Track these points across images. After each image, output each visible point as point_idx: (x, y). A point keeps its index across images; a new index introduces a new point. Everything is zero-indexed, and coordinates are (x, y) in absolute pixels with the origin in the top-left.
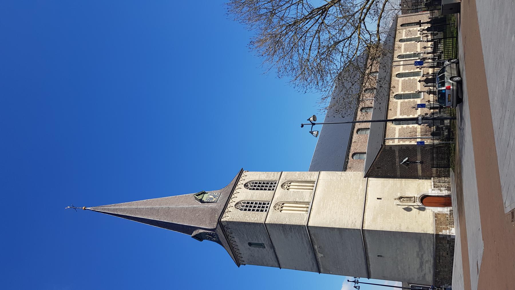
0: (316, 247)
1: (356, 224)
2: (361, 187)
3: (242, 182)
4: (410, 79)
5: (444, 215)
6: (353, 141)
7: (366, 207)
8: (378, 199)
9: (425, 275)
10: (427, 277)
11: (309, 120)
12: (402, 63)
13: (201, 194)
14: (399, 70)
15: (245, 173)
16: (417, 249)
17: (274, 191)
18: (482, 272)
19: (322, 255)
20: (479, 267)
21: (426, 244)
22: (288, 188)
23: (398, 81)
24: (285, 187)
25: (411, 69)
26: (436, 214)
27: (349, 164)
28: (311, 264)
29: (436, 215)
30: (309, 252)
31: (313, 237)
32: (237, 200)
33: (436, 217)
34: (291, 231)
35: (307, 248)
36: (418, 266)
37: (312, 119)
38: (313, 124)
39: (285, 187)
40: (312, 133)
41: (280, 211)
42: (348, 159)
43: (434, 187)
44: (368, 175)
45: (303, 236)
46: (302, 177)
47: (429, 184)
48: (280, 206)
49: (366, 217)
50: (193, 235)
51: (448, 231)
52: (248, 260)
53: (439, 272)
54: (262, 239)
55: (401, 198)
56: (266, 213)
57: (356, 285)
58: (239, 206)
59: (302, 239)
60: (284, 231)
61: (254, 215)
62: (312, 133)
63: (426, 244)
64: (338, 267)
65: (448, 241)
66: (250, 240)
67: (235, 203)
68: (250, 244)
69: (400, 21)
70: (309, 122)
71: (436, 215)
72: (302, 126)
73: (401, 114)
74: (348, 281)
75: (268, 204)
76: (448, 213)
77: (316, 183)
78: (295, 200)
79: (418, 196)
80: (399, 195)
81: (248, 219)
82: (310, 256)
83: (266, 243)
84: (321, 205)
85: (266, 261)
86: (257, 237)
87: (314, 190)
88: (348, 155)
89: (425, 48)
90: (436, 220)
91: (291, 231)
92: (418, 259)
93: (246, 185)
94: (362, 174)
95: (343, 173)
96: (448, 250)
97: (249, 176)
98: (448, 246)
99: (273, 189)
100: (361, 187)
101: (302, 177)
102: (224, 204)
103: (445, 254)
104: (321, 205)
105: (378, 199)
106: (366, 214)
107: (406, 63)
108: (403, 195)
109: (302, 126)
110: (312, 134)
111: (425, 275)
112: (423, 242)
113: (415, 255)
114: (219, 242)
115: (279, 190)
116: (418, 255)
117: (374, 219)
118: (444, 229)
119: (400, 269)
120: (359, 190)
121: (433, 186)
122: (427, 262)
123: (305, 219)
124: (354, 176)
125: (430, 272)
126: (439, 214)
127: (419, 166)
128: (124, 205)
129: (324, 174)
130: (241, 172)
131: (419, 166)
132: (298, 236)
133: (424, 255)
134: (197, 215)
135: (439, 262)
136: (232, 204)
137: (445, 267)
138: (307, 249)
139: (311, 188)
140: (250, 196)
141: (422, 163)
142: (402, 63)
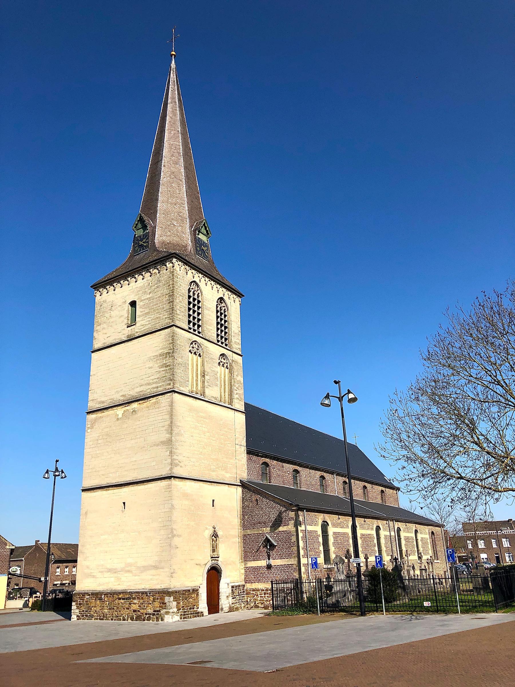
0: (135, 405)
1: (178, 467)
2: (228, 475)
3: (227, 295)
4: (375, 546)
5: (196, 604)
6: (284, 464)
7: (201, 484)
8: (213, 501)
9: (94, 577)
10: (91, 580)
11: (349, 392)
12: (393, 534)
13: (207, 231)
14: (385, 530)
15: (238, 300)
16: (141, 563)
17: (216, 342)
18: (197, 669)
19: (120, 416)
20: (208, 665)
21: (150, 577)
22: (221, 364)
23: (372, 529)
24: (223, 360)
25: (386, 547)
26: (198, 590)
27: (254, 458)
28: (103, 399)
29: (195, 591)
30: (123, 396)
31: (153, 400)
32: (202, 285)
33: (193, 590)
34: (162, 367)
35: (134, 393)
36: (109, 566)
37: (351, 396)
38: (341, 399)
39: (223, 360)
40: (327, 397)
41: (190, 351)
42: (262, 457)
43: (233, 587)
44: (243, 485)
45: (154, 386)
46: (237, 385)
47: (236, 579)
48: (196, 350)
49: (188, 482)
50: (143, 215)
51: (175, 610)
52: (105, 301)
53: (101, 599)
54: (143, 323)
55: (215, 535)
56: (187, 328)
57: (51, 474)
58: (193, 286)
59: (149, 384)
60: (160, 355)
61: (183, 310)
62: (327, 397)
63: (150, 577)
64: (99, 442)
65: (159, 611)
66: (142, 303)
67: (198, 281)
68: (133, 304)
69: (436, 530)
70: (344, 392)
71: (195, 591)
72: (336, 382)
73: (334, 533)
74: (57, 461)
75: (199, 333)
76: (200, 610)
77: (230, 406)
78: (206, 373)
79: (219, 563)
80: (220, 533)
81: (178, 301)
82: (118, 398)
83: (137, 329)
84: (201, 414)
85: (104, 328)
86: (148, 313)
87: (220, 404)
88: (266, 457)
89: (413, 568)
90: (189, 591)
91: (162, 367)
92: (122, 565)
93: (221, 299)
94: (244, 475)
95: (244, 449)
96: (142, 611)
97: (234, 305)
98: (150, 611)
99: (218, 341)
100: (228, 475)
101: (237, 385)
102: (196, 264)
103: (135, 607)
104: (201, 414)
105: (213, 501)
106: (192, 483)
107: (393, 538)
108: (220, 540)
109: (336, 382)
110: (325, 397)
111: (94, 577)
112: (153, 572)
113: (129, 560)
114: (132, 256)
115: (216, 350)
116: (130, 565)
117: (186, 496)
118: (178, 603)
119: (103, 537)
120: (223, 473)
121: (233, 584)
122: (119, 579)
123: (182, 388)
124: (238, 464)
125: (100, 585)
126: (198, 595)
127: (263, 563)
128: (174, 112)
129: (241, 418)
130: (239, 295)
131: (263, 563)
132: (152, 378)
133: (131, 575)
134: (175, 223)
135: (120, 599)
136: (198, 277)
137: (110, 609)
138: (131, 393)
139: (223, 400)
140: (209, 306)
141: (269, 567)
142: (393, 534)
